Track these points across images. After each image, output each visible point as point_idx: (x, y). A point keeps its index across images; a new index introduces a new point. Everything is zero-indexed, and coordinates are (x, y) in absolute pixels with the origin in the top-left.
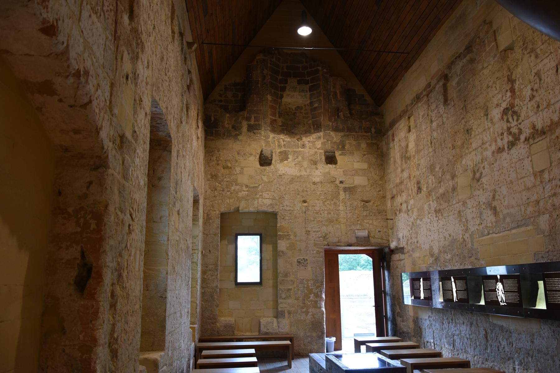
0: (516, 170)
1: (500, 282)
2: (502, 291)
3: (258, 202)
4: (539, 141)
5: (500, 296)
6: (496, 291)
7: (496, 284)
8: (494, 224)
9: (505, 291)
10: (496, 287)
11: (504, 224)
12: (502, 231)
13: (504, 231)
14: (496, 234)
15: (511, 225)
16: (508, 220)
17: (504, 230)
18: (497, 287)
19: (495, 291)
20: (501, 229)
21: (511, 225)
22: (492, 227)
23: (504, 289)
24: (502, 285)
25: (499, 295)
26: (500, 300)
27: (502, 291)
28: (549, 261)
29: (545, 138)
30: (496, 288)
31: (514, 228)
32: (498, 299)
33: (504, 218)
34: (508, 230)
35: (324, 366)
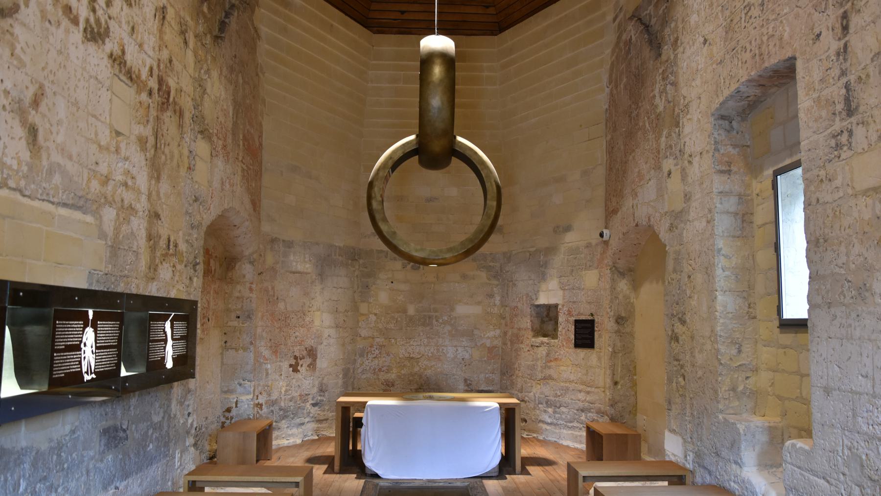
0: (88, 94)
1: (92, 327)
2: (92, 347)
3: (30, 458)
4: (124, 82)
5: (86, 360)
6: (80, 349)
7: (83, 331)
8: (25, 169)
9: (97, 348)
10: (82, 338)
11: (48, 184)
12: (39, 196)
13: (43, 200)
14: (24, 196)
15: (60, 195)
16: (57, 179)
17: (44, 197)
18: (84, 340)
19: (77, 348)
20: (40, 191)
21: (60, 195)
22: (17, 171)
23: (96, 343)
24: (93, 334)
25: (85, 358)
26: (84, 369)
27: (92, 347)
28: (106, 290)
29: (129, 86)
30: (81, 342)
31: (65, 205)
32: (81, 367)
33: (50, 172)
34: (53, 203)
35: (205, 4)
